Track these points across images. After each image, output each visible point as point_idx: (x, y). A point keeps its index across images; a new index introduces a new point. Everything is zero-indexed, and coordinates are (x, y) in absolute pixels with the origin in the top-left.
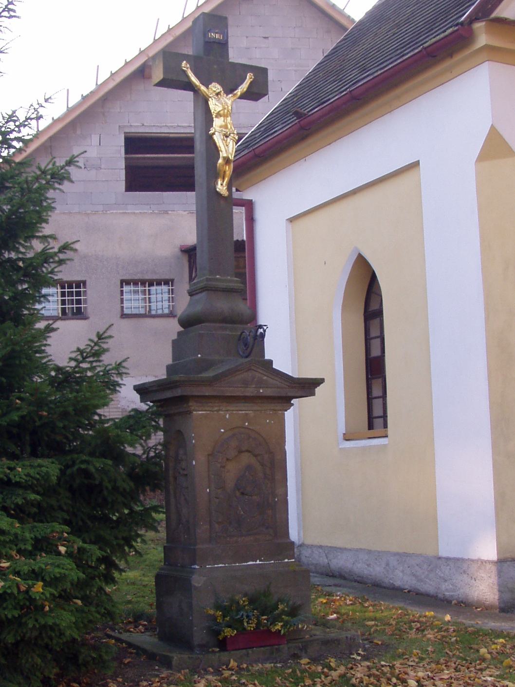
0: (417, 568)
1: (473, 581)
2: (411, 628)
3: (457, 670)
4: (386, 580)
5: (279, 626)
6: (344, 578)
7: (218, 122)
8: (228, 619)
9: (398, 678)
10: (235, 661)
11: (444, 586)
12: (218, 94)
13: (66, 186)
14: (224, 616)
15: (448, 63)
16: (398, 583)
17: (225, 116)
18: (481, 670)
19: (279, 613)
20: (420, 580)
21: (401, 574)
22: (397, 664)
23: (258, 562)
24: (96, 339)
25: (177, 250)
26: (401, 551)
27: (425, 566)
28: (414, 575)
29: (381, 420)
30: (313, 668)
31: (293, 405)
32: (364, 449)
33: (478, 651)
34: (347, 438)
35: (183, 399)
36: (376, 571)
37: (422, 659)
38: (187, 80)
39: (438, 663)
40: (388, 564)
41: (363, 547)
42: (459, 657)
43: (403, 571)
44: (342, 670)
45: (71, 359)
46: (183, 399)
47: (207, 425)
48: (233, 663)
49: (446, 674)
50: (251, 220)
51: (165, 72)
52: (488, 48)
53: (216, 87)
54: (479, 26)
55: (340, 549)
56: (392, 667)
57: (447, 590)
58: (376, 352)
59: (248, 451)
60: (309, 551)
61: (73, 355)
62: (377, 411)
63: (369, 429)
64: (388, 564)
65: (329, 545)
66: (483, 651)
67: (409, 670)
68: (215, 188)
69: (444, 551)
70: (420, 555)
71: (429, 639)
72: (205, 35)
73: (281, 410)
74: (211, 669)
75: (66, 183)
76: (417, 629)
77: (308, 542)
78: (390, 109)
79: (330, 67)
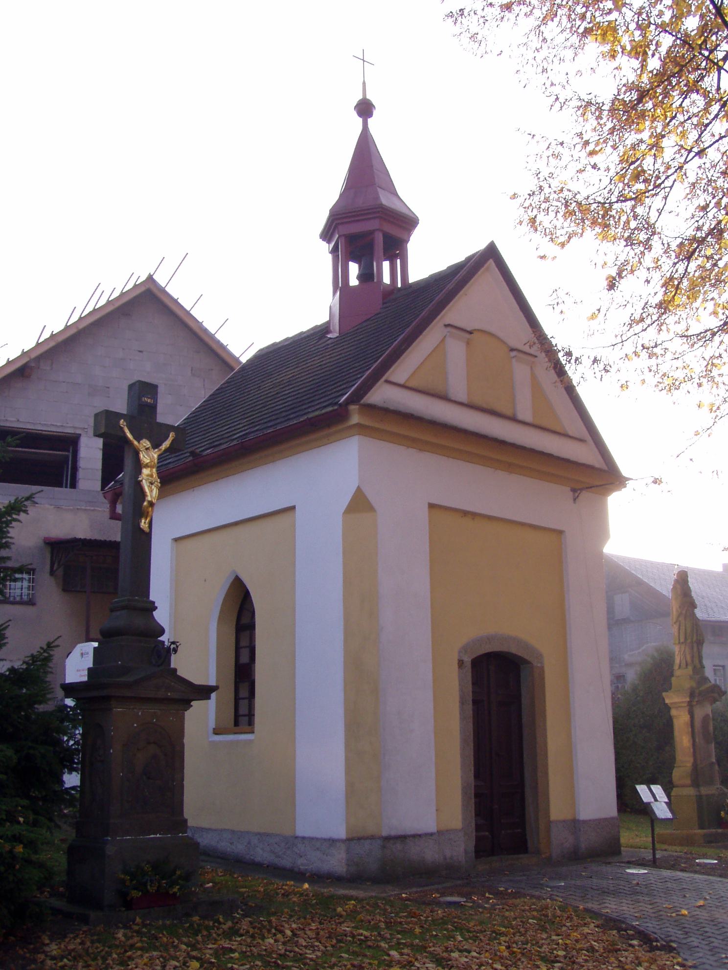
0: (276, 846)
2: (278, 894)
3: (321, 923)
4: (248, 857)
5: (176, 889)
6: (209, 855)
7: (146, 471)
8: (134, 882)
9: (276, 930)
10: (140, 918)
11: (300, 861)
12: (147, 449)
13: (22, 516)
14: (131, 880)
16: (258, 859)
17: (152, 467)
18: (340, 923)
22: (273, 919)
24: (45, 647)
26: (262, 831)
29: (247, 718)
30: (206, 922)
33: (335, 910)
34: (216, 732)
35: (108, 698)
36: (239, 848)
37: (291, 916)
39: (305, 918)
40: (249, 843)
41: (227, 827)
42: (321, 915)
43: (262, 849)
44: (229, 924)
45: (24, 662)
46: (108, 698)
47: (124, 720)
48: (138, 920)
49: (314, 926)
52: (359, 426)
53: (146, 443)
54: (353, 408)
56: (270, 922)
57: (302, 865)
58: (244, 659)
59: (154, 743)
61: (27, 659)
62: (244, 710)
64: (249, 843)
66: (339, 909)
67: (284, 923)
68: (139, 525)
69: (303, 829)
71: (294, 902)
72: (140, 399)
74: (121, 925)
75: (22, 514)
76: (283, 894)
79: (215, 408)
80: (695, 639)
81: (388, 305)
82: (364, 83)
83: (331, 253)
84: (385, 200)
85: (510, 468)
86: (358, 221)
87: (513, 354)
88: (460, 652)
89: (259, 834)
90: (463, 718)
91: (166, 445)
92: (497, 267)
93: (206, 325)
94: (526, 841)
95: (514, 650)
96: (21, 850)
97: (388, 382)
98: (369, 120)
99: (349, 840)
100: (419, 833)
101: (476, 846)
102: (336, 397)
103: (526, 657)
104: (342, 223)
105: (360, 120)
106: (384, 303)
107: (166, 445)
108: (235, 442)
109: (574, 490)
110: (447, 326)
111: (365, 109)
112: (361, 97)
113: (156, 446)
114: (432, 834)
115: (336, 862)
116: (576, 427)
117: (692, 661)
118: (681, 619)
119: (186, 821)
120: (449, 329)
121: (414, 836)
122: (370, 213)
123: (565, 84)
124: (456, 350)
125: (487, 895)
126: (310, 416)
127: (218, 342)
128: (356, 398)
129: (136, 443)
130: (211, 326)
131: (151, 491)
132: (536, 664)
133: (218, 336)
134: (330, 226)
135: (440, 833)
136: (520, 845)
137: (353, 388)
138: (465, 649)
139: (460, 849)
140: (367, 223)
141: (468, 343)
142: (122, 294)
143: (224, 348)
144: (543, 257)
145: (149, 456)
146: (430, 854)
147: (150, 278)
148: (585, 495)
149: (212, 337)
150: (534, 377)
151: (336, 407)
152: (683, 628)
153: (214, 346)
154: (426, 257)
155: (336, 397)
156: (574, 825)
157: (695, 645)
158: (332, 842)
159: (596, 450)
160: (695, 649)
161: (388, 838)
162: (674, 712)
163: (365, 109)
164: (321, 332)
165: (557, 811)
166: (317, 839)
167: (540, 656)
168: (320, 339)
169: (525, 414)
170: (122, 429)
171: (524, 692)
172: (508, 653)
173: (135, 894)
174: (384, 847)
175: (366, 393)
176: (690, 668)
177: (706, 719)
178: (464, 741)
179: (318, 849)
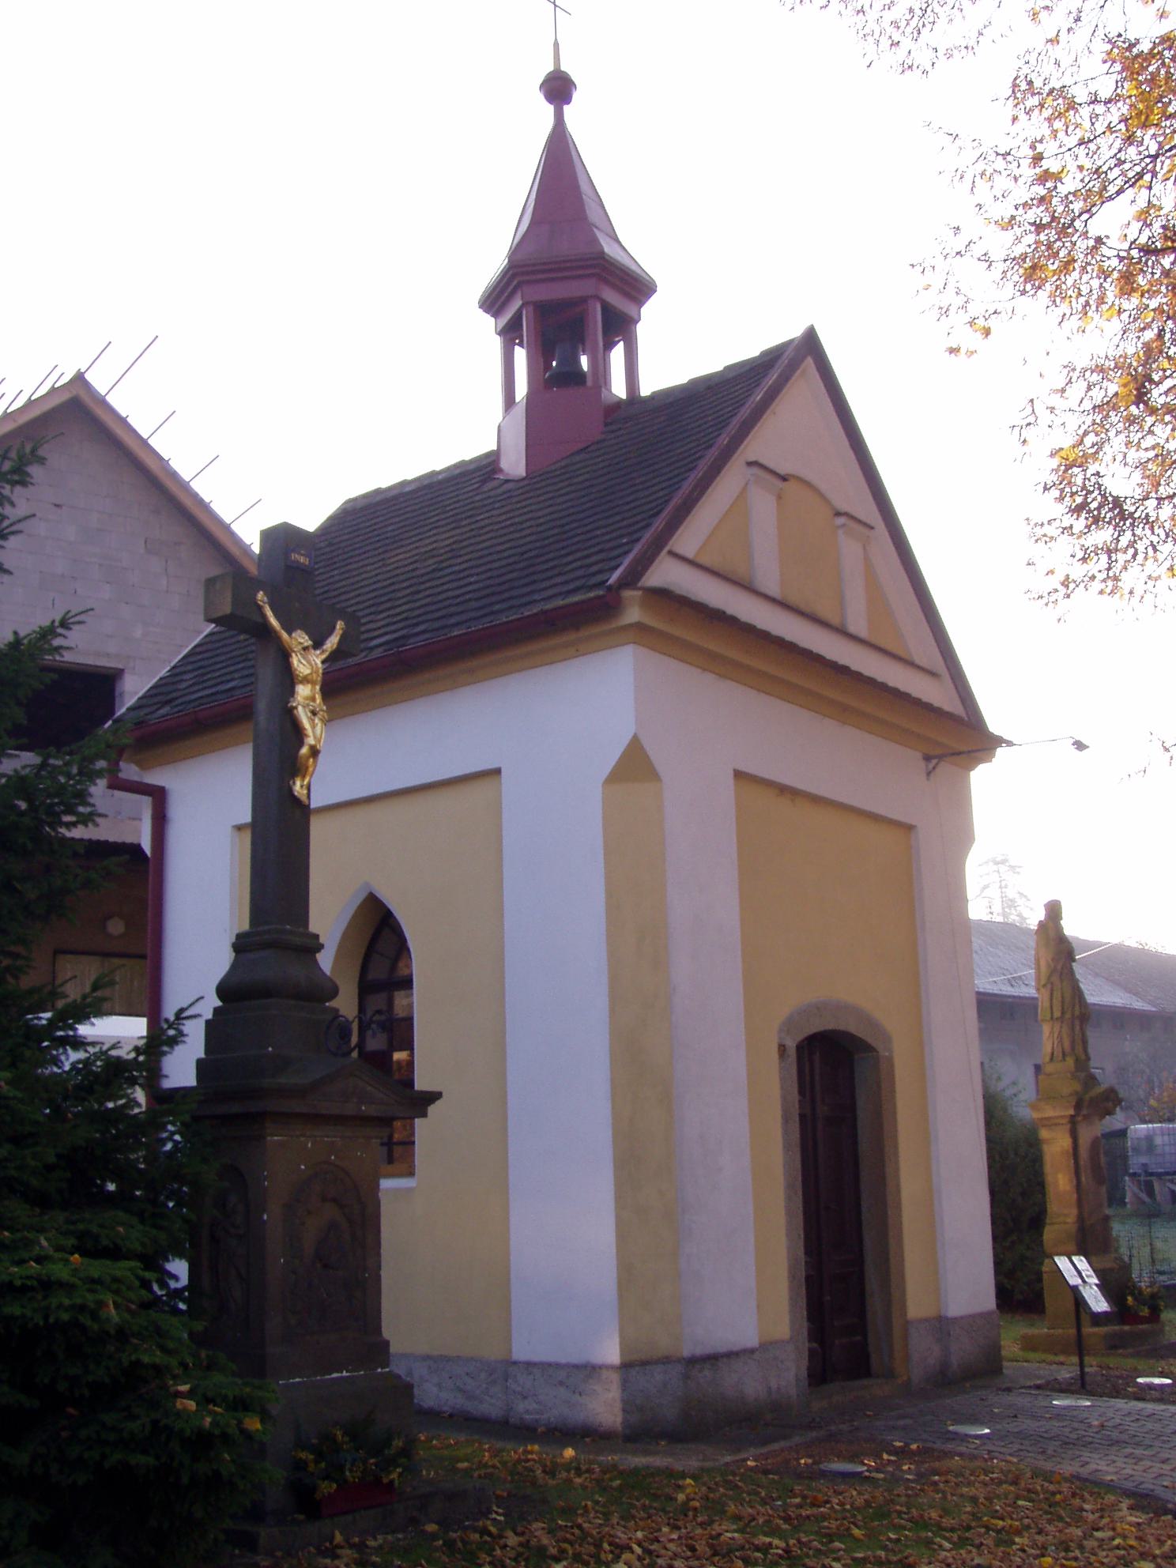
1: (577, 1396)
7: (303, 691)
8: (323, 1465)
12: (305, 649)
14: (317, 1462)
15: (572, 636)
17: (313, 683)
19: (379, 1456)
21: (435, 1390)
23: (345, 1374)
27: (483, 1375)
28: (460, 1390)
38: (260, 620)
43: (439, 1386)
47: (286, 1157)
50: (160, 820)
51: (235, 602)
52: (639, 627)
53: (301, 638)
54: (627, 594)
59: (334, 1200)
68: (291, 791)
69: (523, 1349)
78: (454, 685)
80: (1077, 1013)
81: (614, 427)
82: (556, 45)
83: (499, 334)
84: (609, 249)
85: (843, 713)
86: (552, 280)
87: (841, 520)
88: (780, 1031)
89: (427, 1357)
90: (787, 1147)
91: (332, 642)
92: (818, 370)
93: (176, 465)
94: (868, 1356)
96: (259, 1426)
97: (671, 553)
100: (735, 1349)
102: (600, 572)
103: (869, 1040)
104: (528, 282)
105: (550, 108)
106: (606, 425)
107: (332, 642)
108: (377, 653)
109: (927, 758)
110: (750, 464)
111: (558, 89)
112: (551, 68)
113: (318, 644)
114: (752, 1351)
116: (924, 652)
117: (1073, 1048)
118: (1055, 979)
119: (387, 1344)
120: (755, 470)
122: (565, 269)
123: (929, 68)
124: (763, 507)
125: (885, 1456)
126: (549, 606)
127: (195, 497)
128: (632, 579)
129: (285, 635)
130: (183, 466)
131: (314, 727)
132: (884, 1053)
133: (196, 486)
134: (508, 284)
135: (764, 1346)
136: (859, 1365)
137: (631, 556)
138: (788, 1025)
139: (788, 1375)
140: (564, 285)
141: (779, 497)
142: (30, 403)
143: (205, 506)
144: (953, 351)
145: (307, 663)
146: (748, 1385)
147: (80, 378)
148: (945, 769)
149: (185, 486)
150: (867, 559)
151: (601, 593)
152: (1057, 995)
153: (188, 502)
154: (669, 351)
155: (600, 572)
156: (941, 1325)
157: (1077, 1023)
159: (953, 692)
160: (1078, 1028)
161: (693, 1361)
162: (1044, 1134)
163: (558, 89)
164: (486, 468)
165: (916, 1305)
166: (558, 1366)
168: (484, 482)
169: (858, 624)
170: (260, 608)
171: (861, 1102)
173: (327, 1488)
174: (686, 1377)
175: (646, 568)
176: (1070, 1061)
177: (1095, 1143)
178: (789, 1186)
179: (561, 1383)
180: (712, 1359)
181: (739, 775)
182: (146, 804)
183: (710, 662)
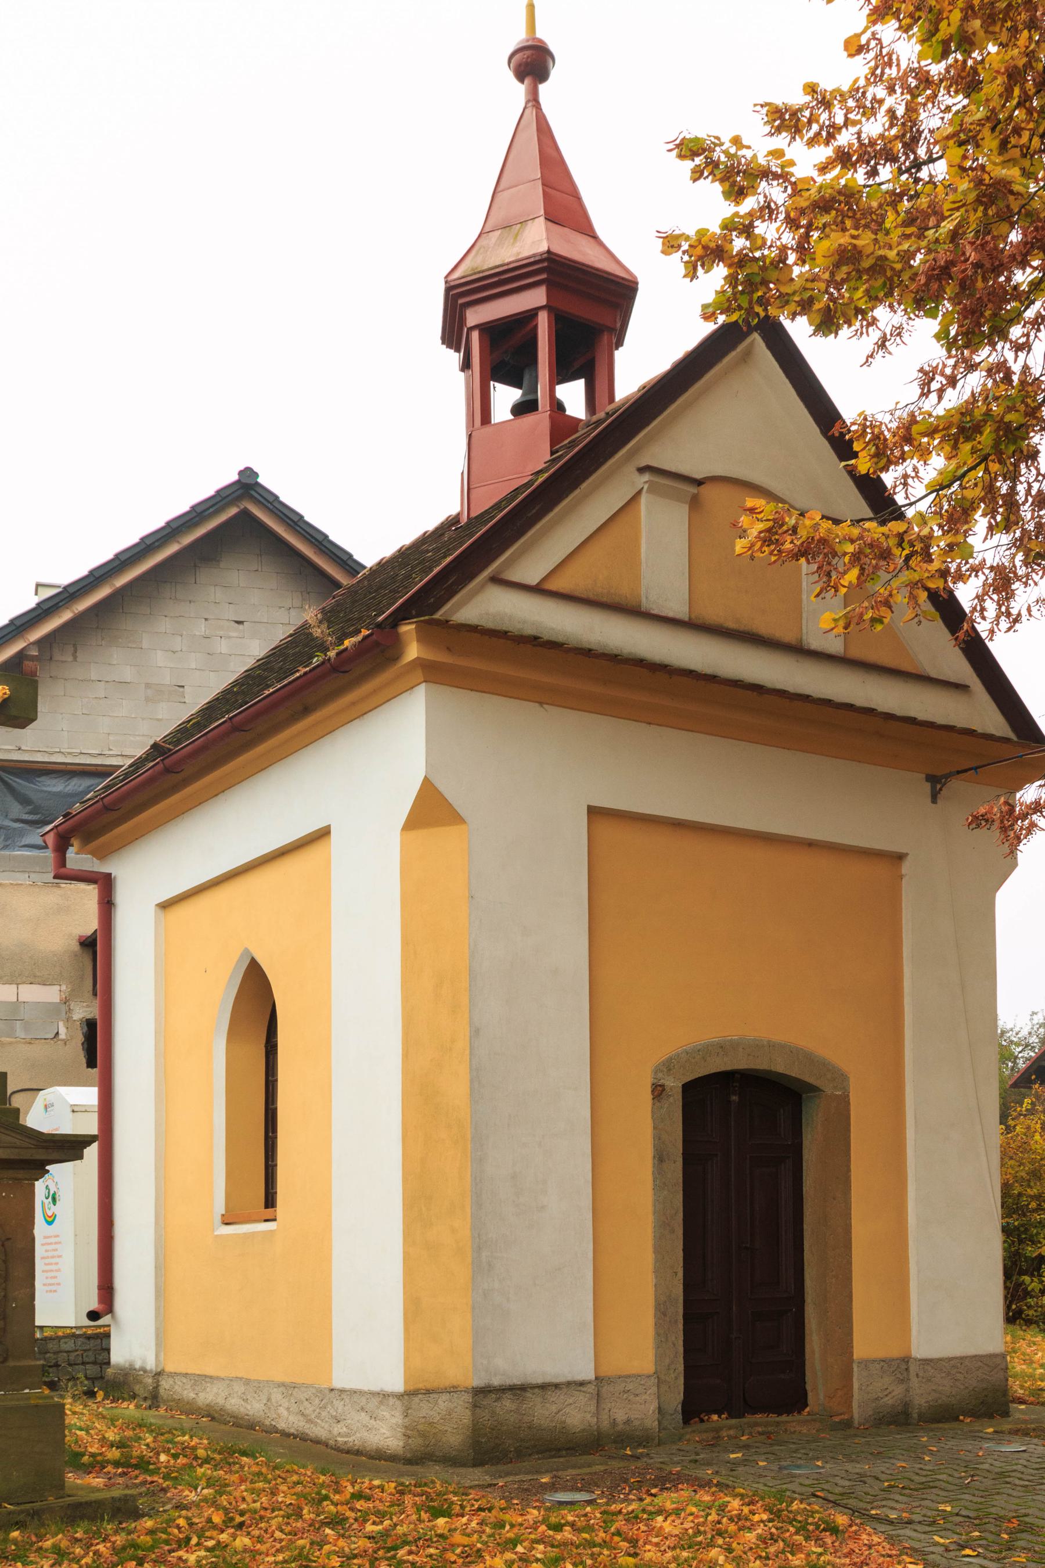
0: (306, 1403)
20: (310, 1421)
21: (285, 1413)
25: (75, 947)
27: (317, 1401)
31: (48, 1171)
32: (247, 1236)
40: (269, 1400)
43: (288, 1409)
55: (211, 1377)
60: (171, 1381)
63: (266, 1207)
64: (269, 1400)
65: (198, 1372)
70: (311, 1386)
73: (26, 1179)
77: (170, 1368)
88: (657, 1070)
89: (283, 1385)
95: (780, 1066)
98: (542, 88)
99: (409, 1394)
101: (684, 1404)
103: (811, 1080)
105: (519, 91)
111: (533, 63)
115: (385, 1432)
120: (647, 477)
121: (544, 1387)
138: (668, 1066)
156: (902, 1366)
158: (384, 1396)
163: (533, 63)
165: (867, 1342)
167: (841, 1078)
172: (770, 1072)
174: (475, 1406)
179: (362, 1409)
180: (518, 1390)
181: (593, 812)
182: (90, 893)
183: (544, 696)
